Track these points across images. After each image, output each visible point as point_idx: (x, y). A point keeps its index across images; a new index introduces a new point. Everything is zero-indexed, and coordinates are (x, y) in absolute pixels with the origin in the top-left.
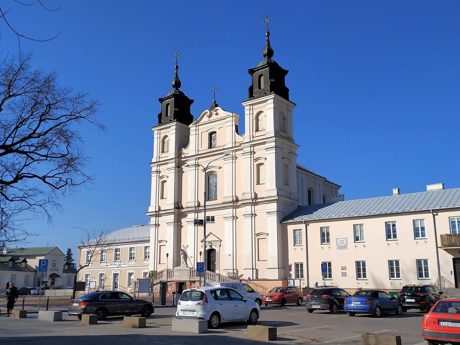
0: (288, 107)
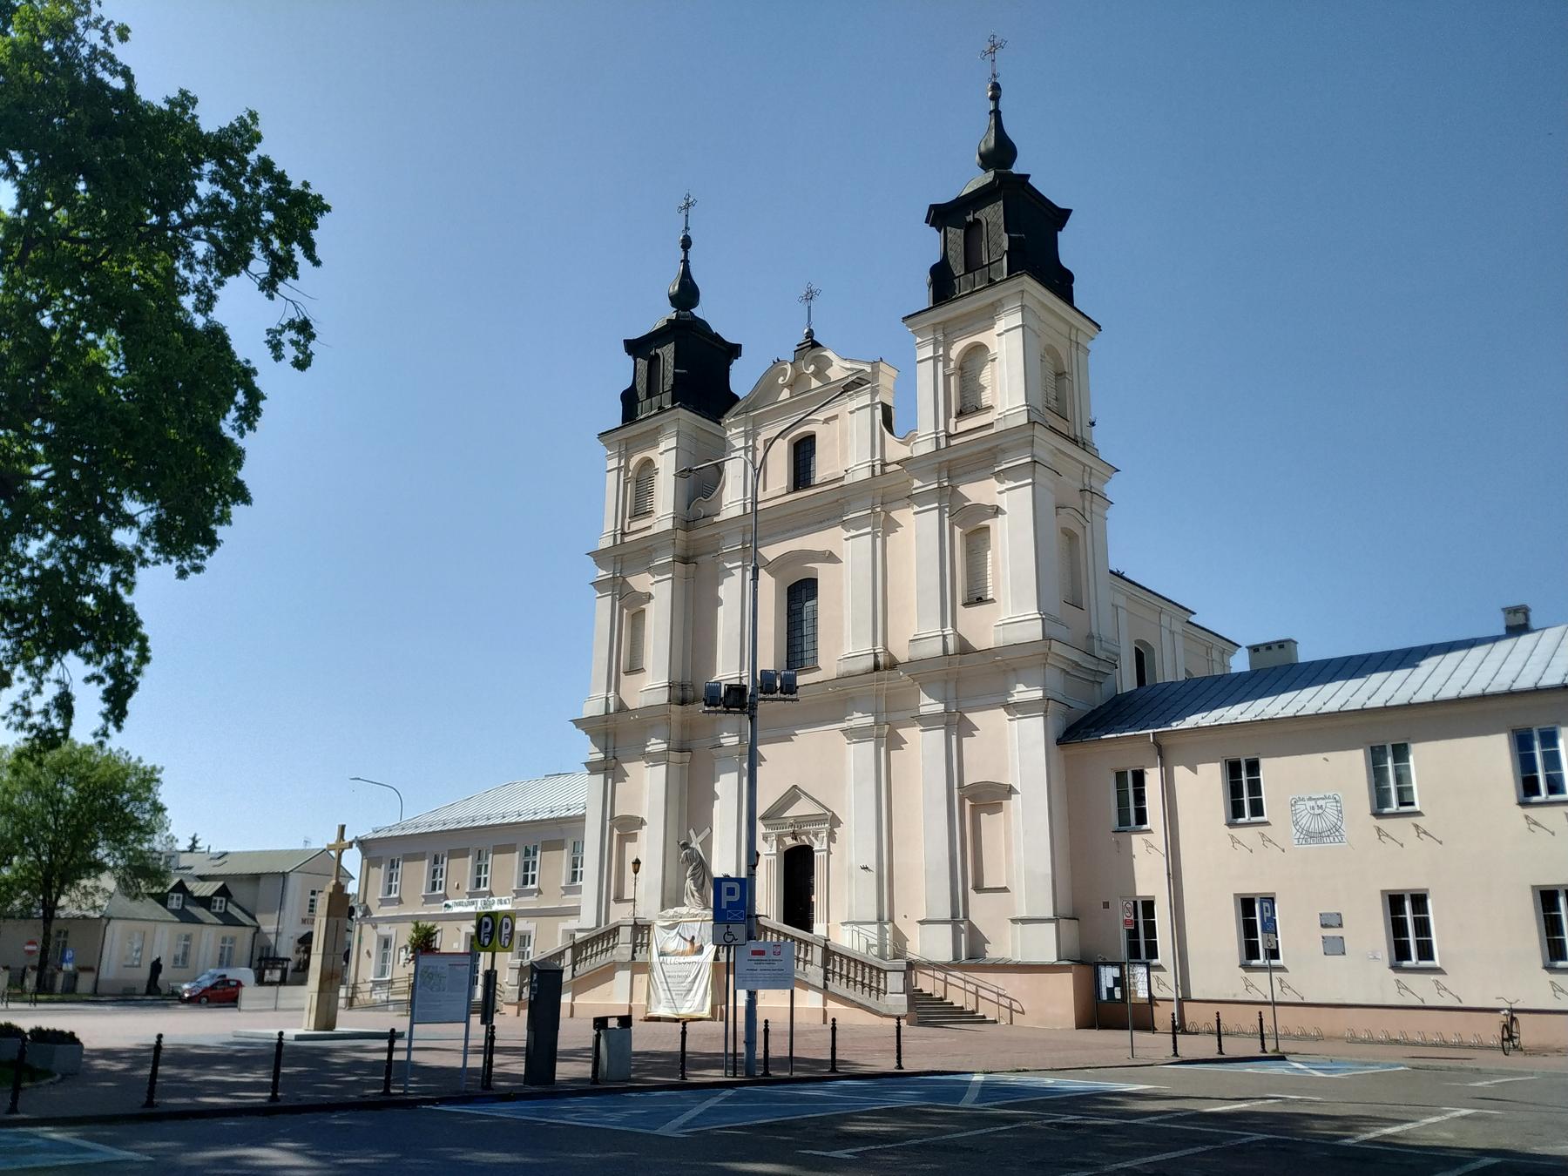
0: (1074, 331)
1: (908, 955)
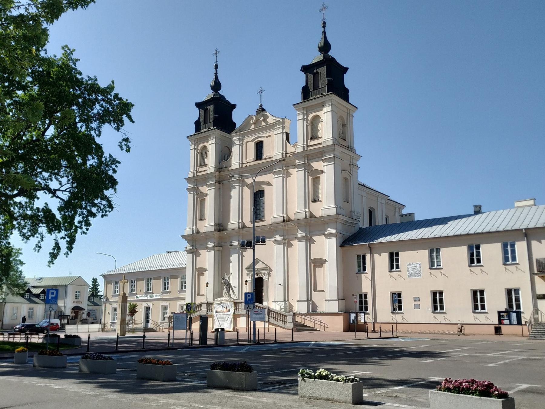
1: (293, 311)
